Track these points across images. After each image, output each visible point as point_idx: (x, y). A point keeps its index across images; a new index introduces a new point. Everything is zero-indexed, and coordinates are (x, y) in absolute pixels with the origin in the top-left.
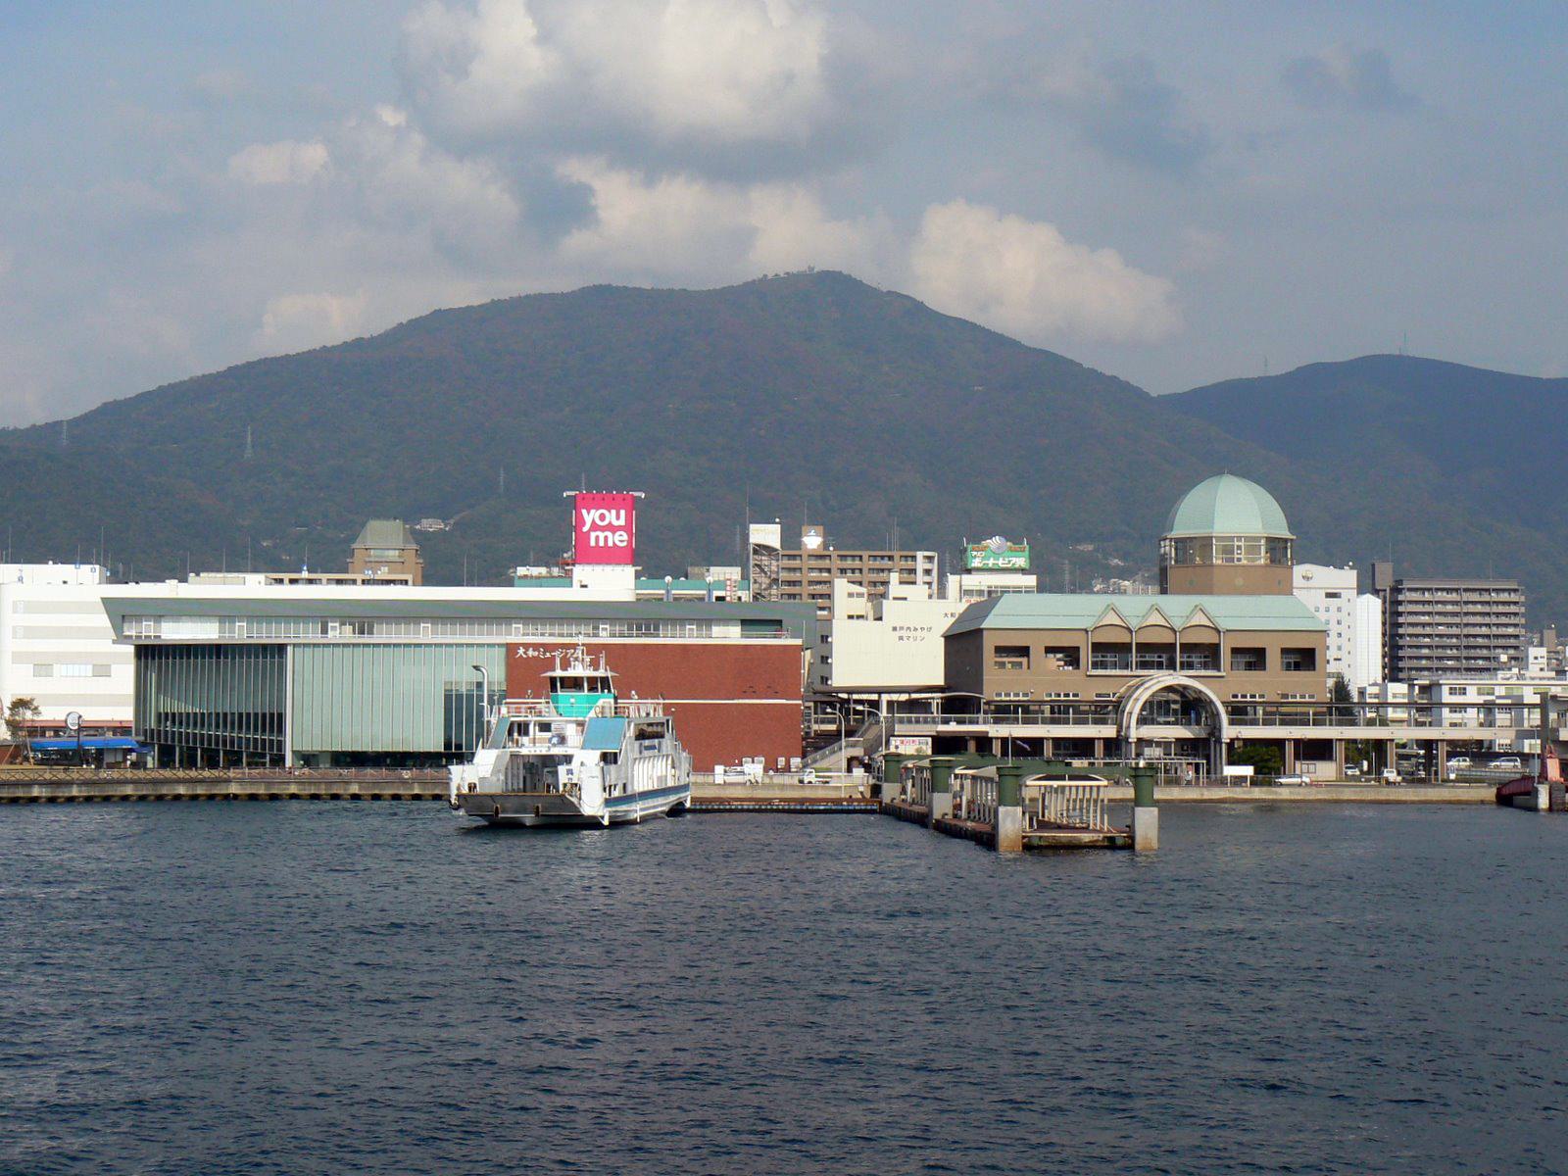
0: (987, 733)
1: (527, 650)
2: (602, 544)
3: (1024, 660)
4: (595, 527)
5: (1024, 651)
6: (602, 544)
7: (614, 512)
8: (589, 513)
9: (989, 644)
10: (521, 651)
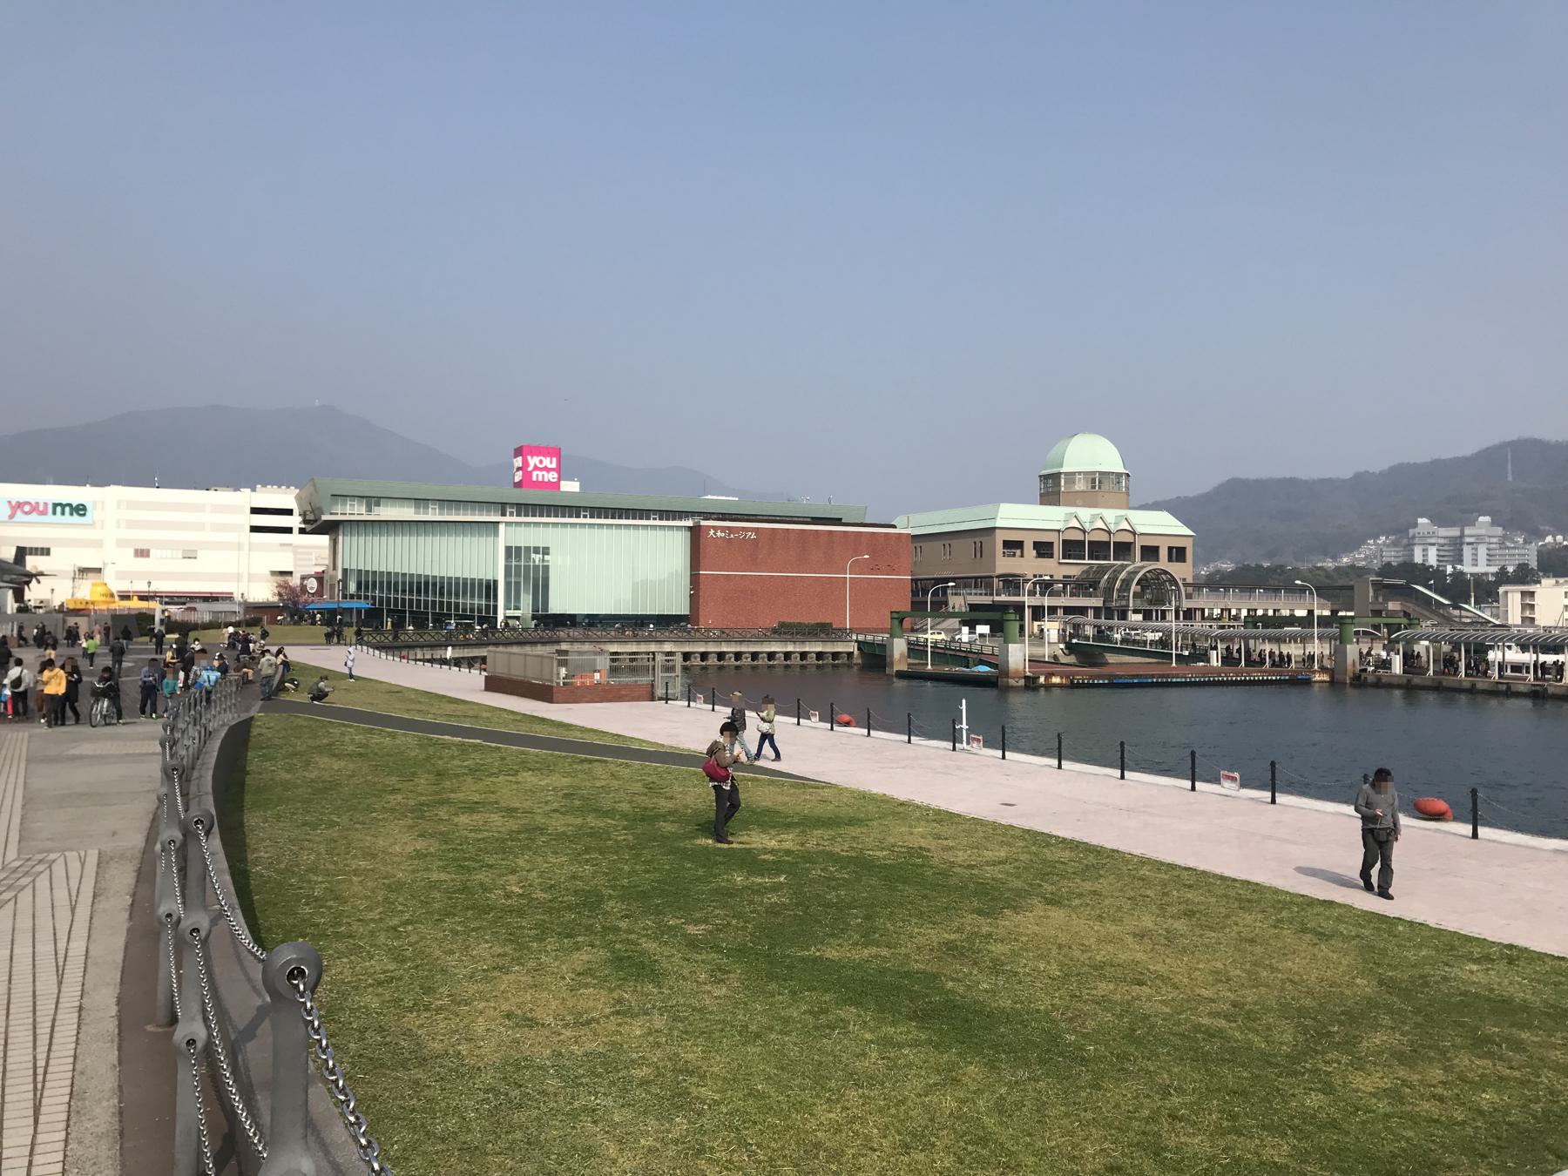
3: (1018, 552)
4: (536, 468)
9: (1000, 537)
10: (712, 532)
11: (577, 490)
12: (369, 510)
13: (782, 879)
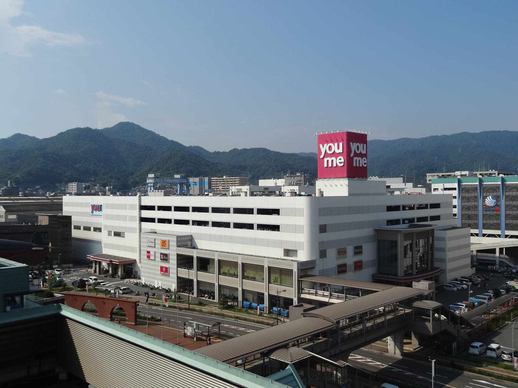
2: (330, 165)
6: (330, 165)
7: (336, 144)
11: (404, 340)
13: (37, 187)
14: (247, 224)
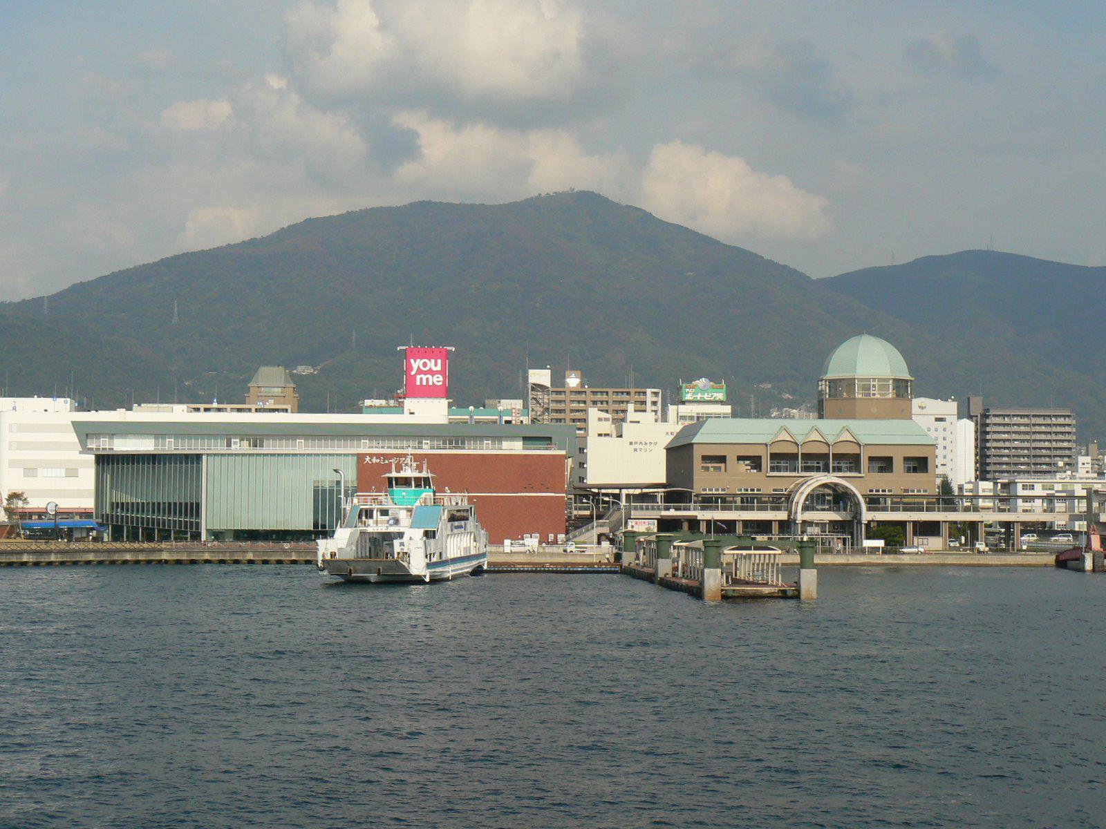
0: (696, 516)
1: (372, 458)
2: (424, 383)
3: (722, 465)
4: (419, 371)
5: (722, 459)
6: (424, 383)
7: (433, 361)
8: (415, 361)
9: (698, 454)
10: (368, 459)
12: (264, 404)
14: (338, 413)
